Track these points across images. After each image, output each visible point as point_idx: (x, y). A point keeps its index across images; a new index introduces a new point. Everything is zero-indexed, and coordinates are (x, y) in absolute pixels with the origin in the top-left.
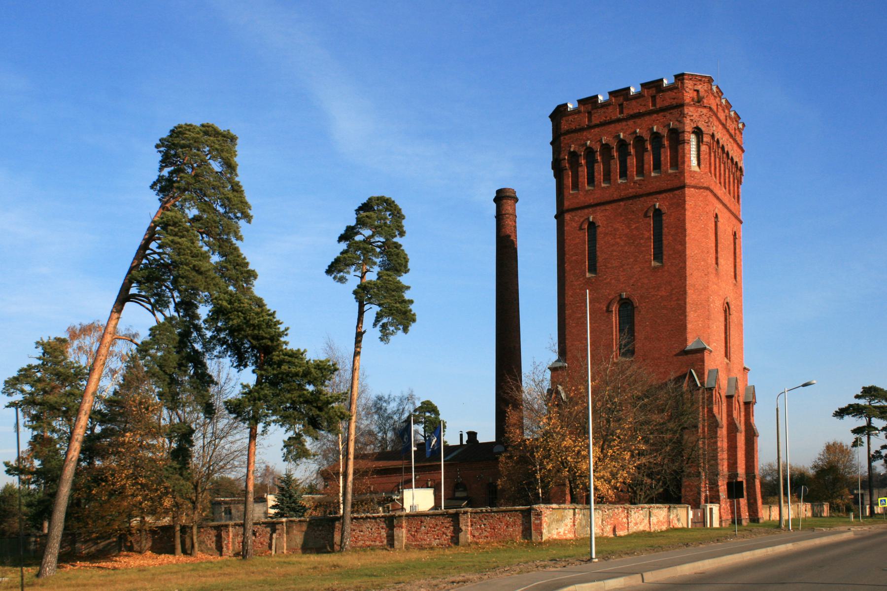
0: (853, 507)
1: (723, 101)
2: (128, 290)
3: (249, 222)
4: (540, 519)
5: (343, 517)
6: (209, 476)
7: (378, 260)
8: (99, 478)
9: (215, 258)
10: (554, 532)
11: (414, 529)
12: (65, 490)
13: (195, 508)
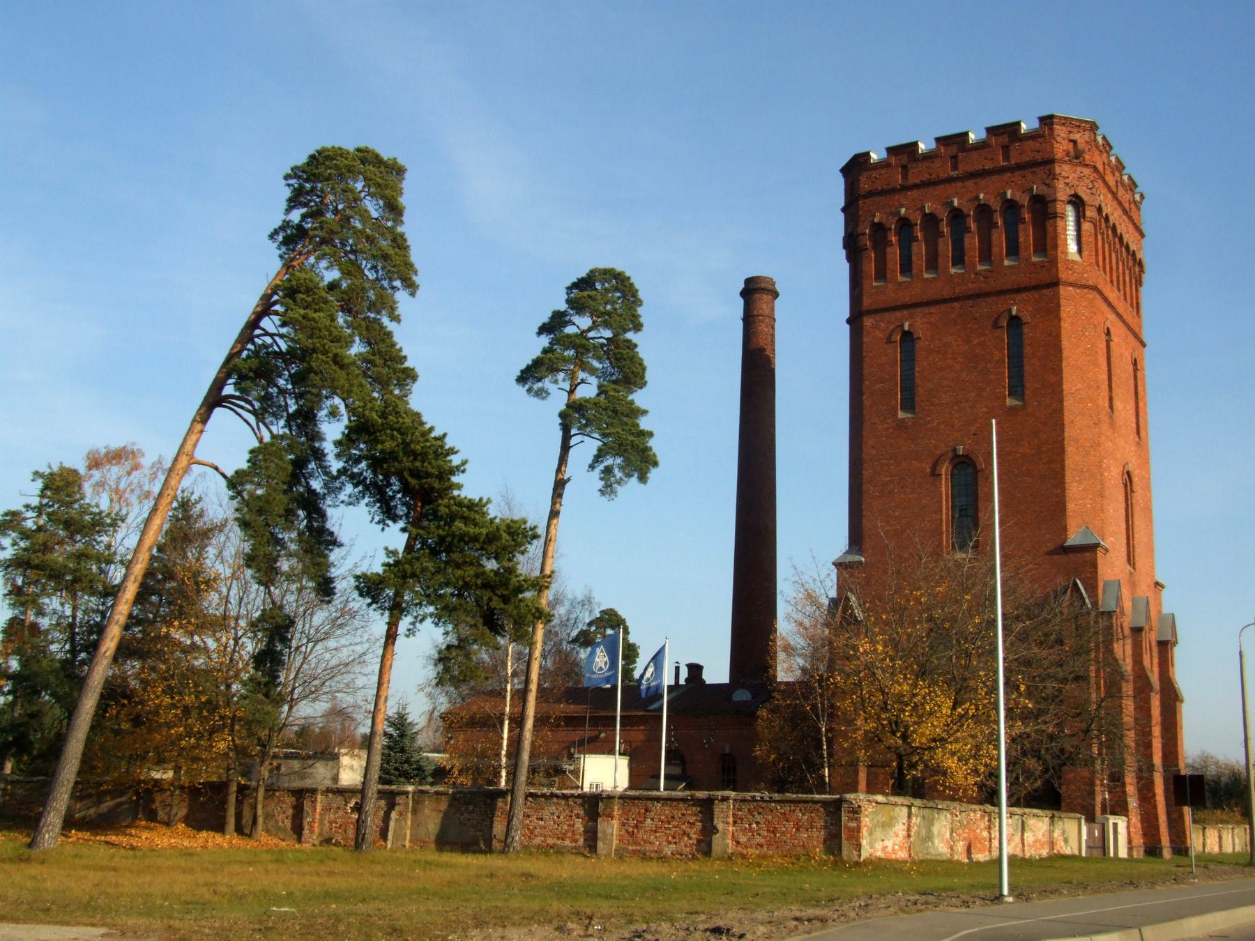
1: (1113, 159)
2: (221, 389)
3: (413, 294)
4: (858, 820)
10: (879, 845)
11: (632, 823)
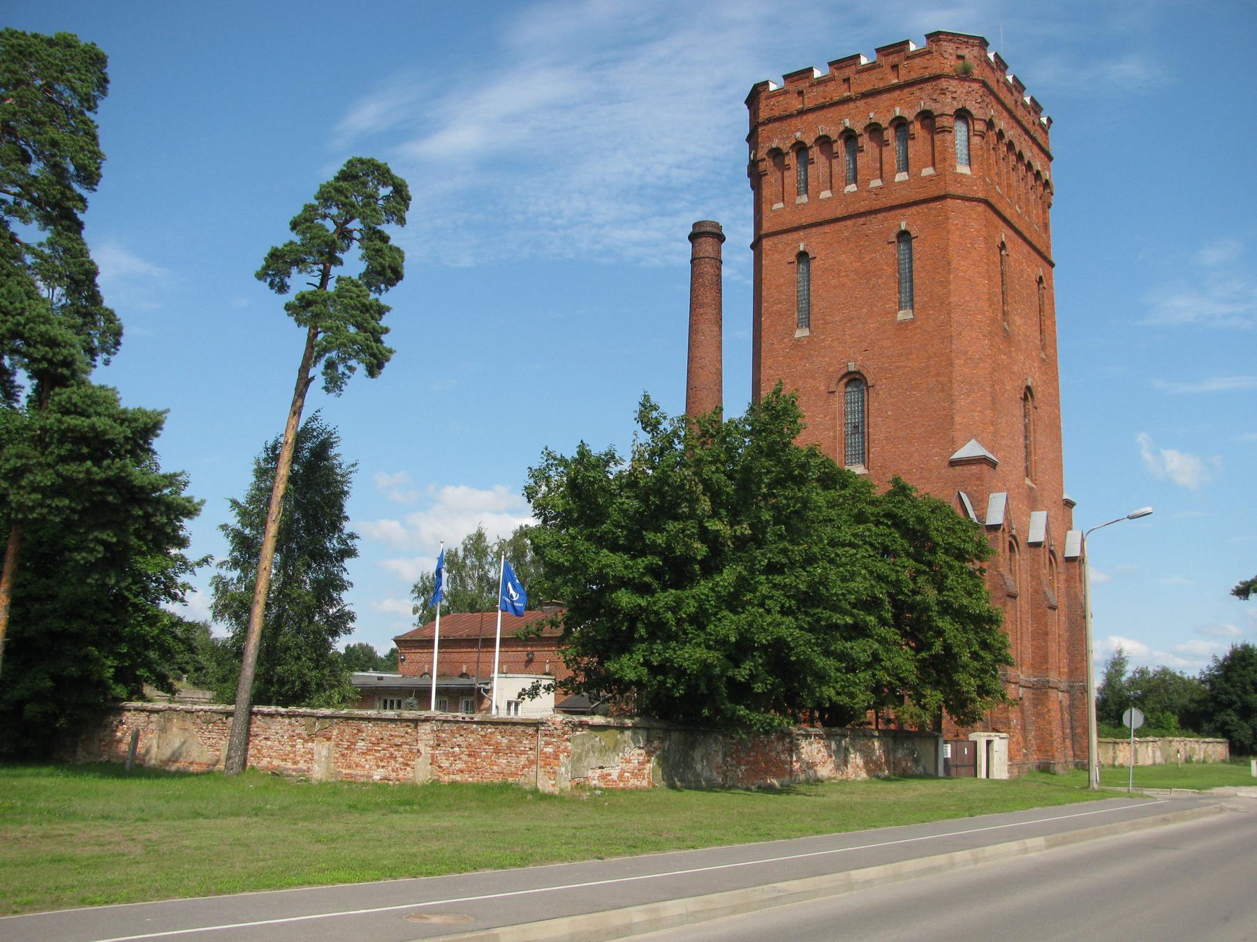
11: (346, 744)
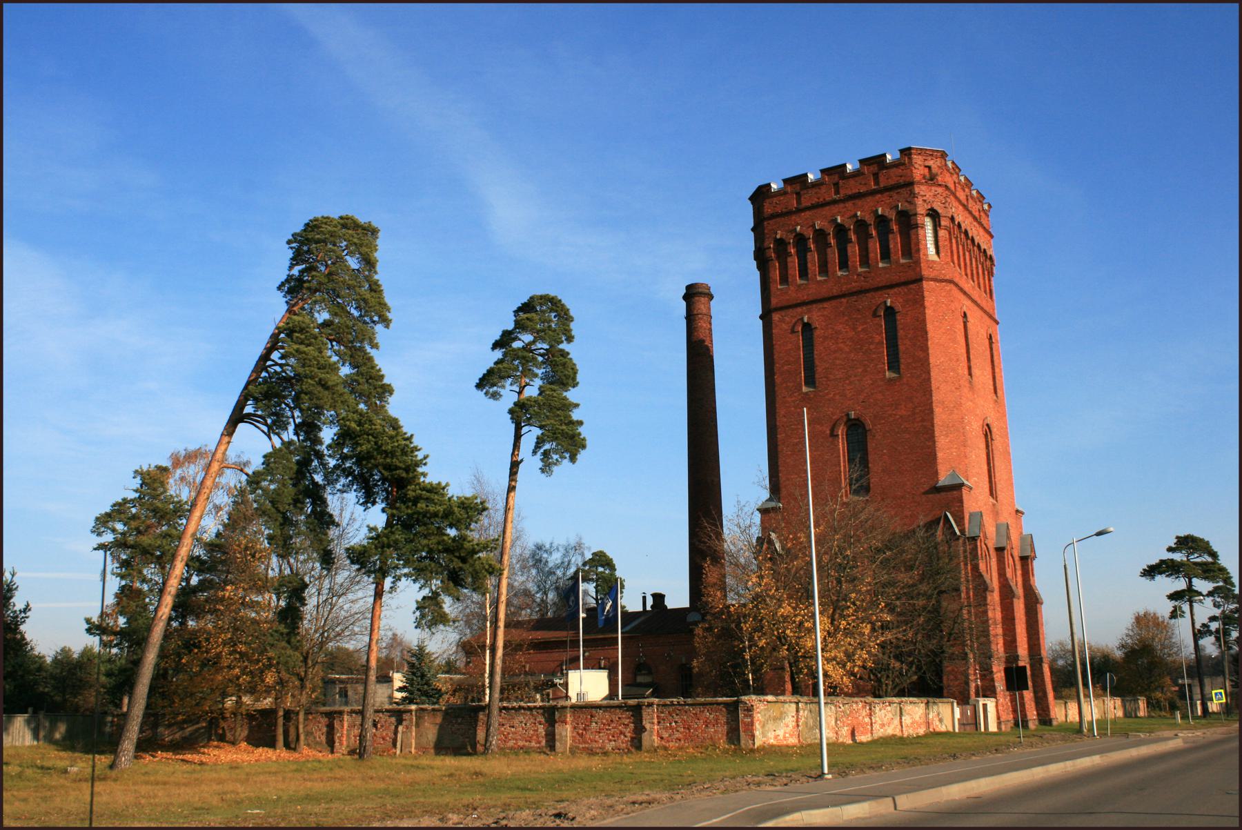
0: (1179, 703)
1: (962, 178)
2: (243, 409)
3: (387, 326)
4: (751, 716)
5: (489, 706)
6: (322, 644)
7: (540, 372)
8: (191, 643)
9: (345, 370)
10: (771, 735)
11: (582, 726)
12: (151, 657)
13: (303, 687)
